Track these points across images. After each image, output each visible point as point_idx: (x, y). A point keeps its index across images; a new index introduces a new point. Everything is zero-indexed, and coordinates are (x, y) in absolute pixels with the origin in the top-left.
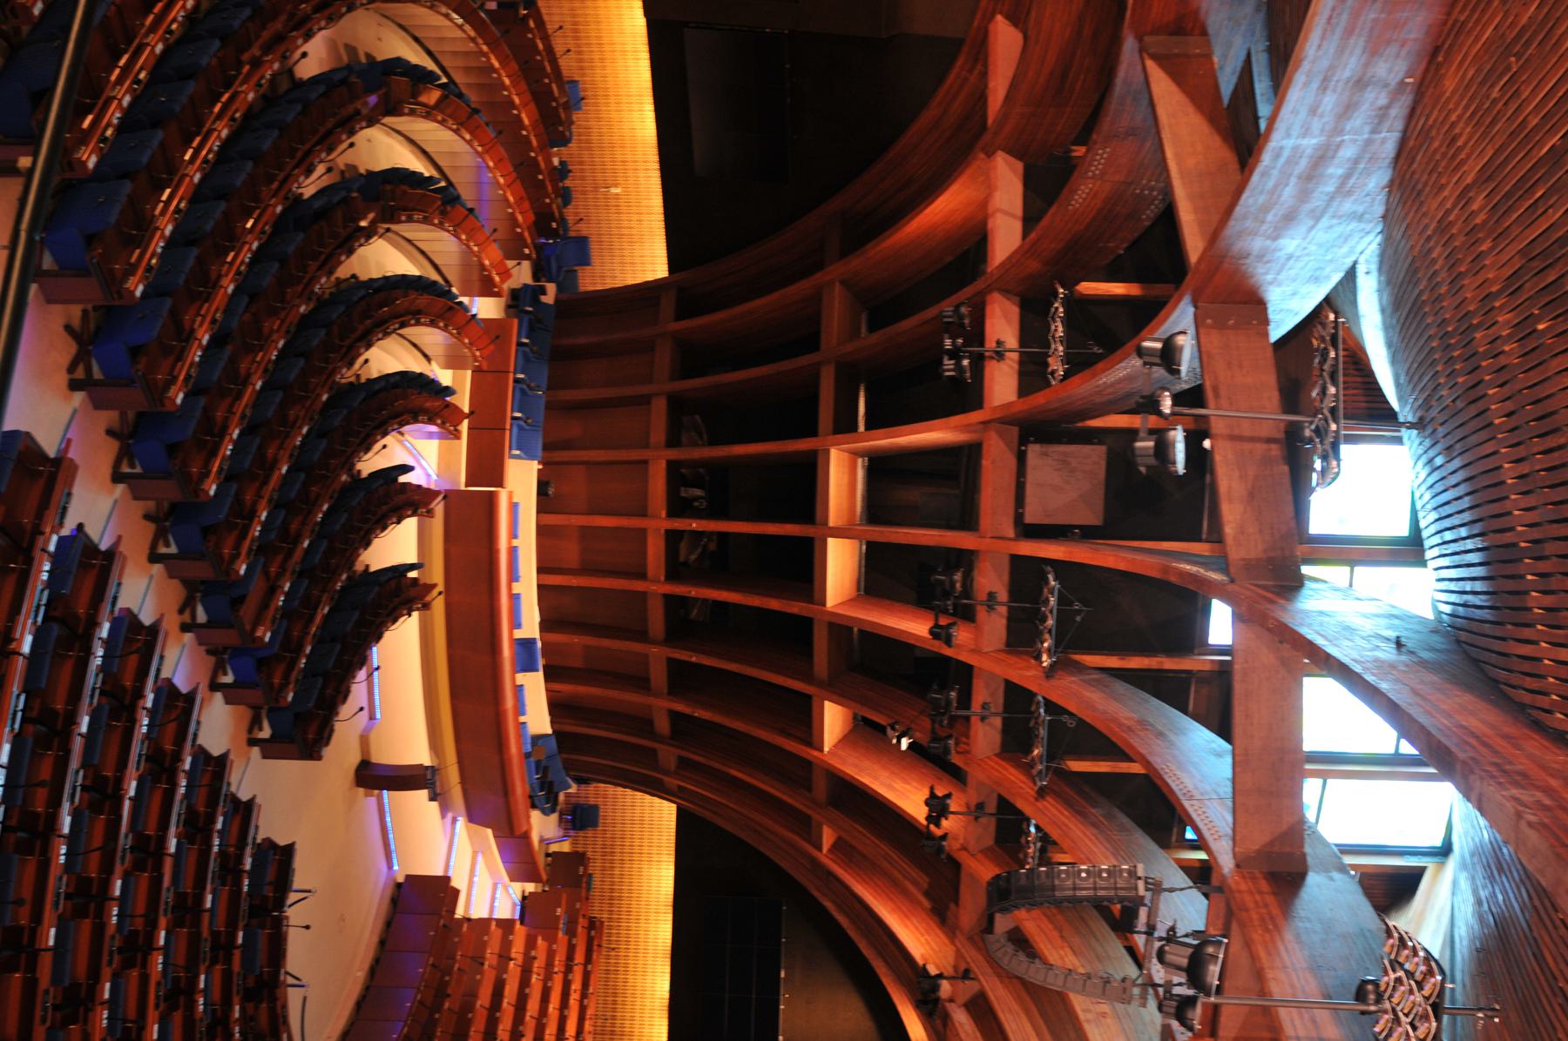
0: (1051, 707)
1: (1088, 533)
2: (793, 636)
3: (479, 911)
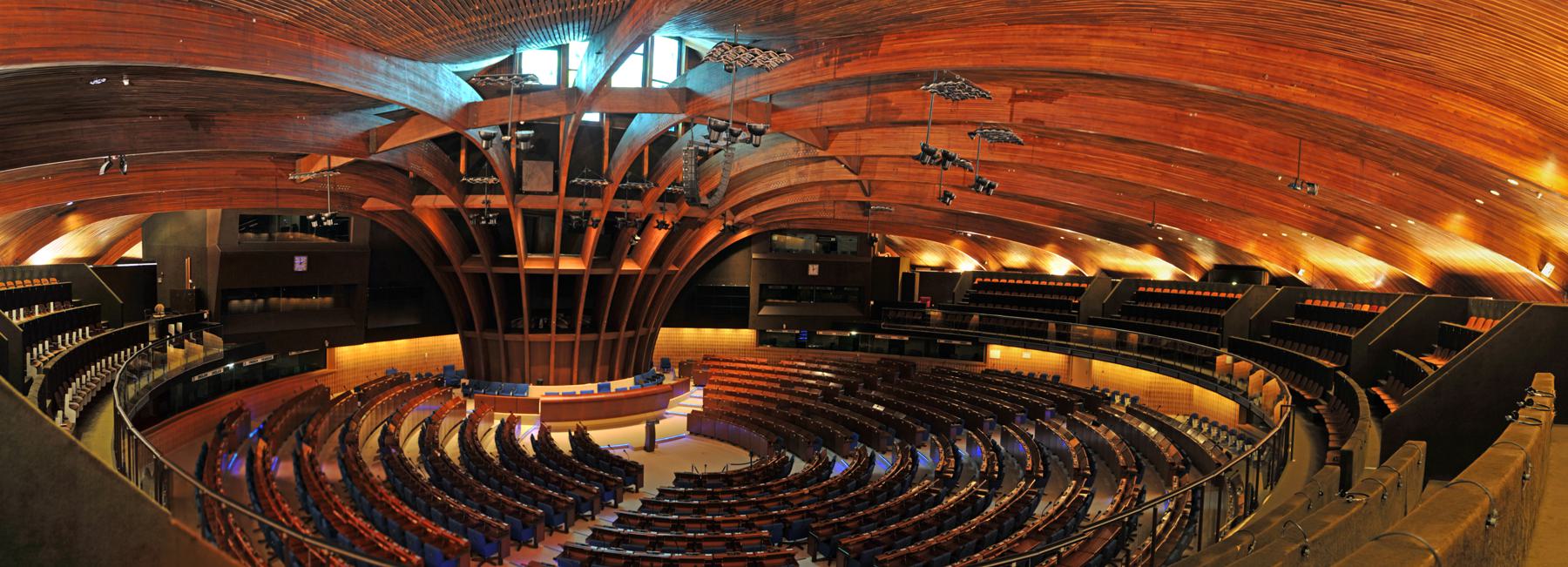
0: (623, 181)
1: (557, 167)
2: (597, 283)
3: (701, 402)
